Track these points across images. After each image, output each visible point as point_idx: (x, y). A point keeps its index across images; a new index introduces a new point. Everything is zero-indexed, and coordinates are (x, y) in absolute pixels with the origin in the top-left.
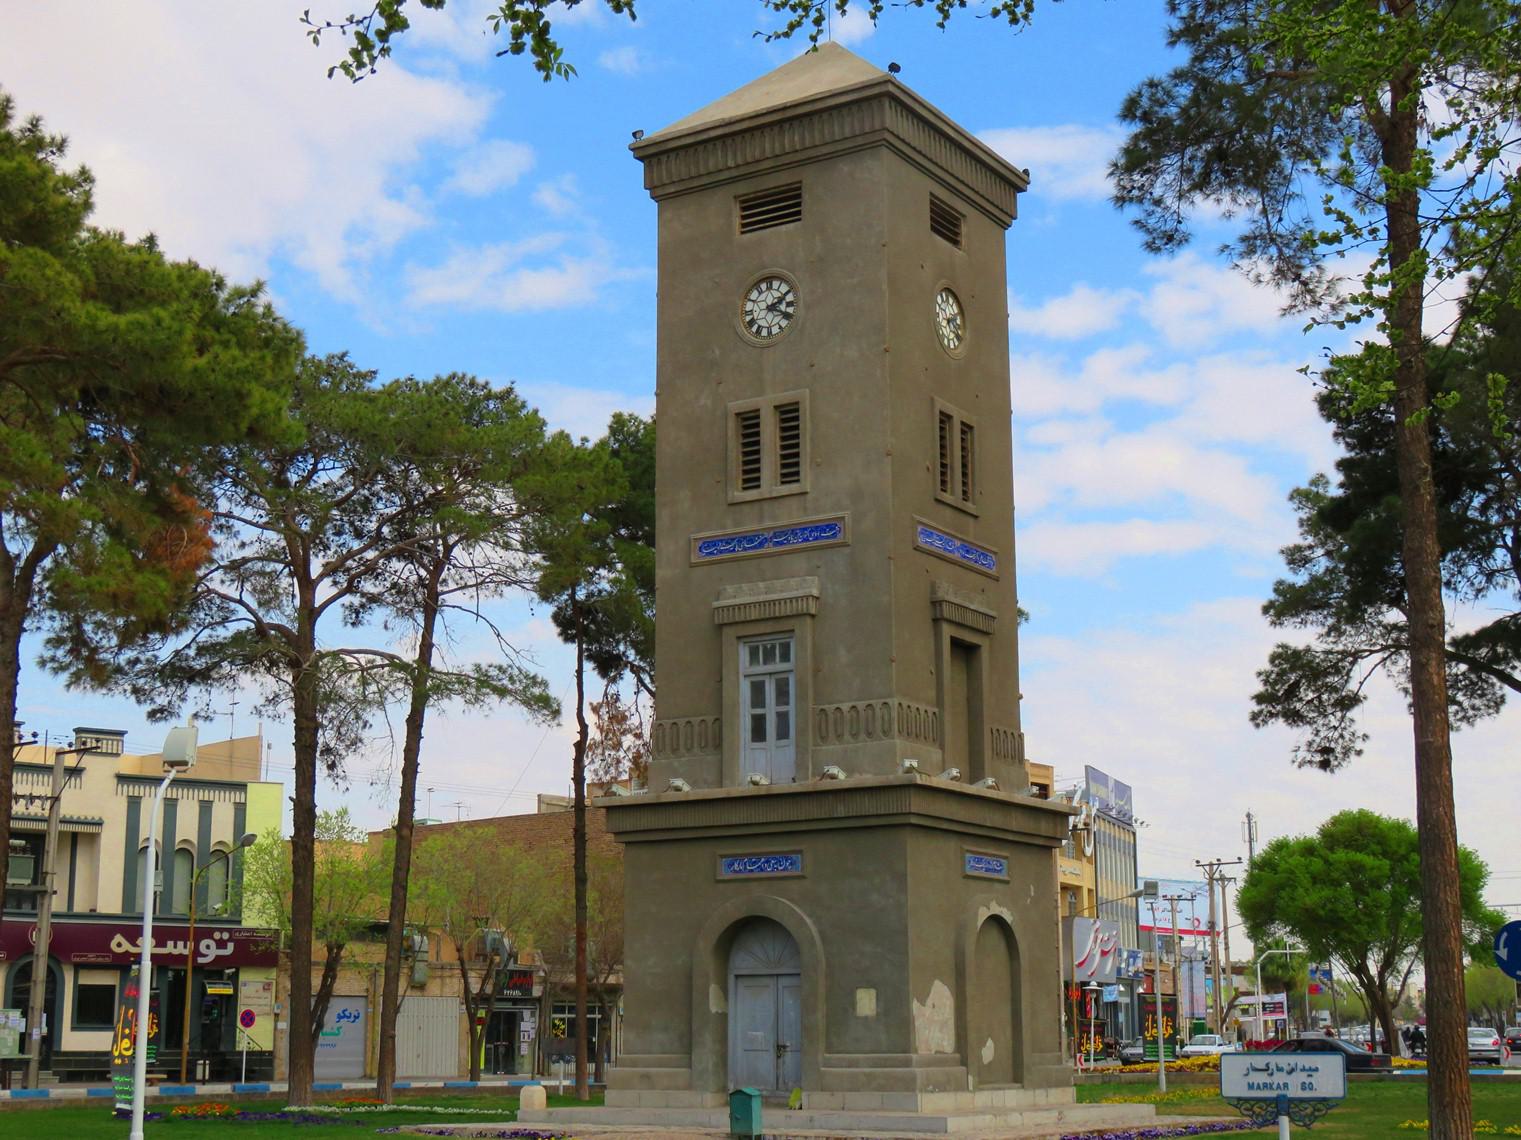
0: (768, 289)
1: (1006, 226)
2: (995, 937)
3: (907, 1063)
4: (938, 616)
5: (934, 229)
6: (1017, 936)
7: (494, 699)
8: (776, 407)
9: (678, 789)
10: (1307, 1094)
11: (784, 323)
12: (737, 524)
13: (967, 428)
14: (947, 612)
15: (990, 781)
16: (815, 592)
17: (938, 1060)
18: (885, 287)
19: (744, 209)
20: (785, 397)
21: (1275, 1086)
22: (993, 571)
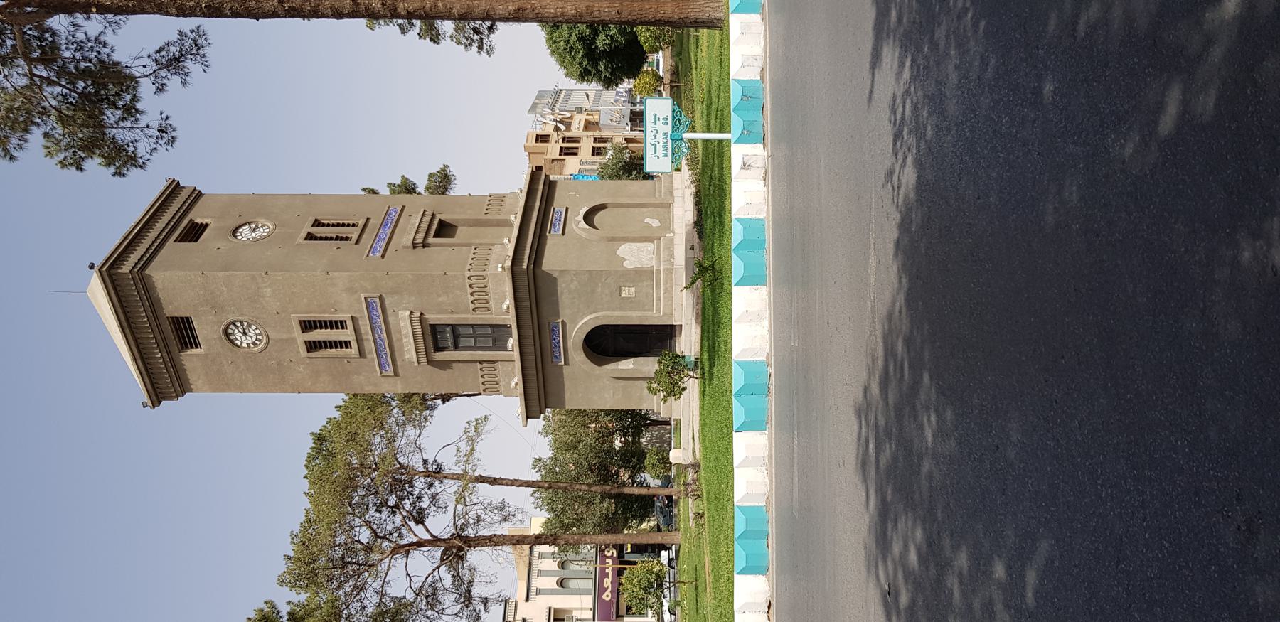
0: (234, 335)
1: (200, 194)
2: (598, 218)
3: (659, 272)
4: (421, 245)
5: (196, 241)
6: (595, 205)
7: (476, 455)
8: (303, 332)
9: (516, 384)
10: (670, 121)
11: (254, 327)
12: (371, 352)
13: (317, 223)
14: (419, 240)
15: (512, 218)
16: (408, 313)
17: (658, 252)
18: (228, 274)
19: (187, 348)
20: (297, 327)
21: (665, 141)
22: (399, 209)
